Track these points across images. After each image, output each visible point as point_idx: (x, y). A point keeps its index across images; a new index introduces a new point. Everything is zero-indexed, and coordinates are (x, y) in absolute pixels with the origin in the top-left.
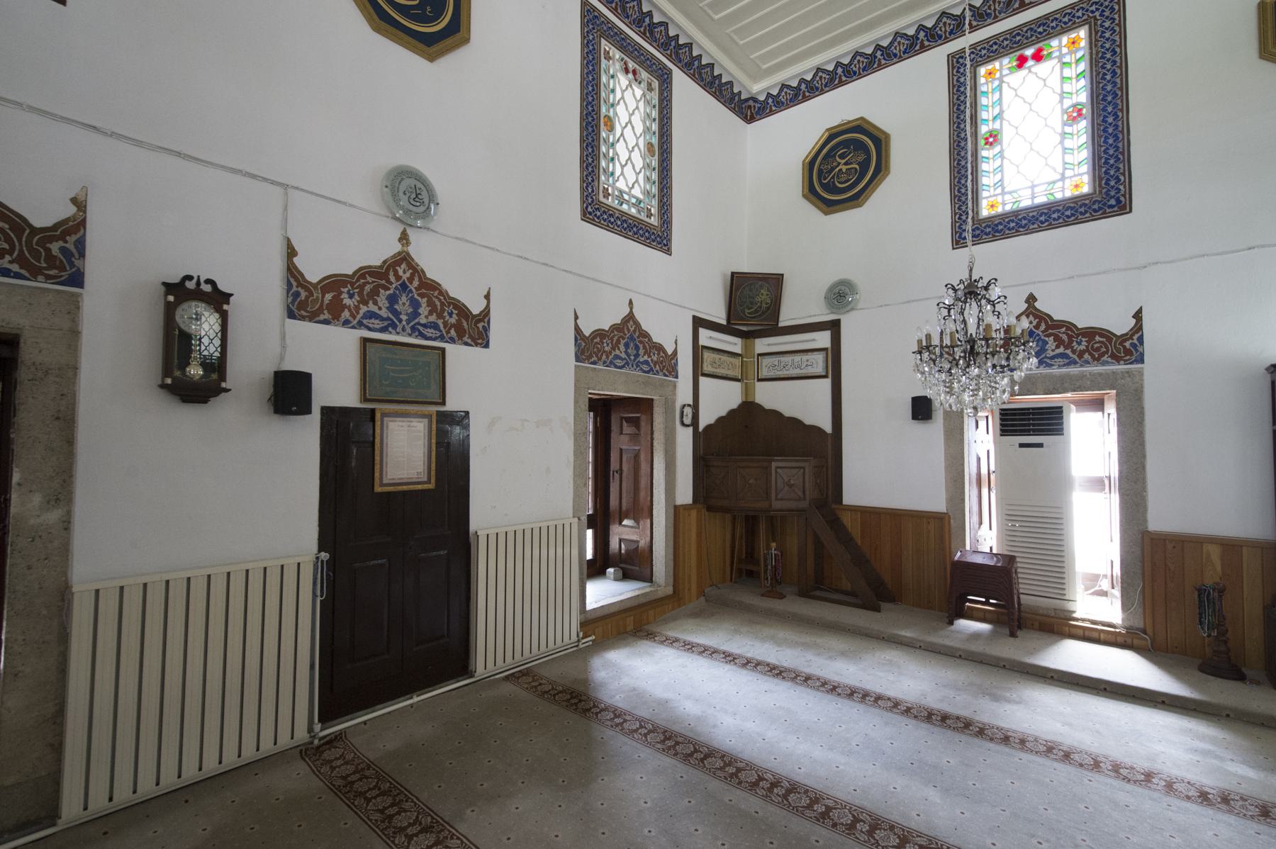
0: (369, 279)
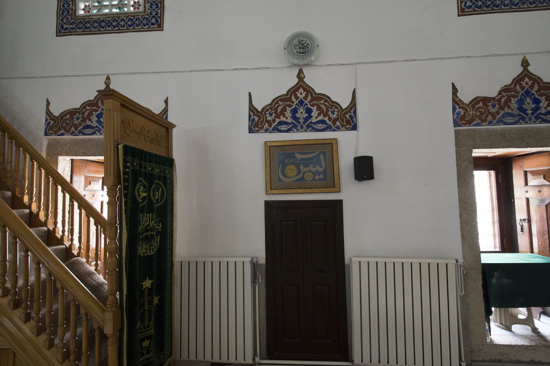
0: (280, 103)
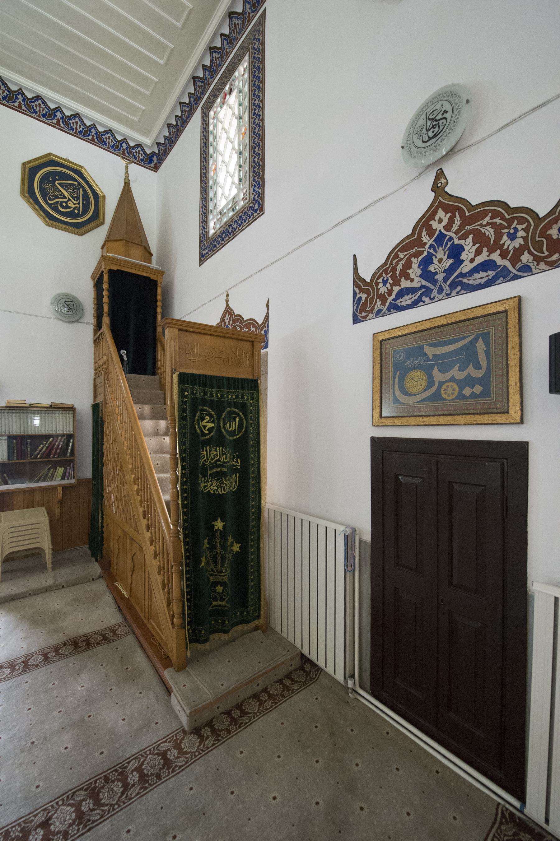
0: (401, 255)
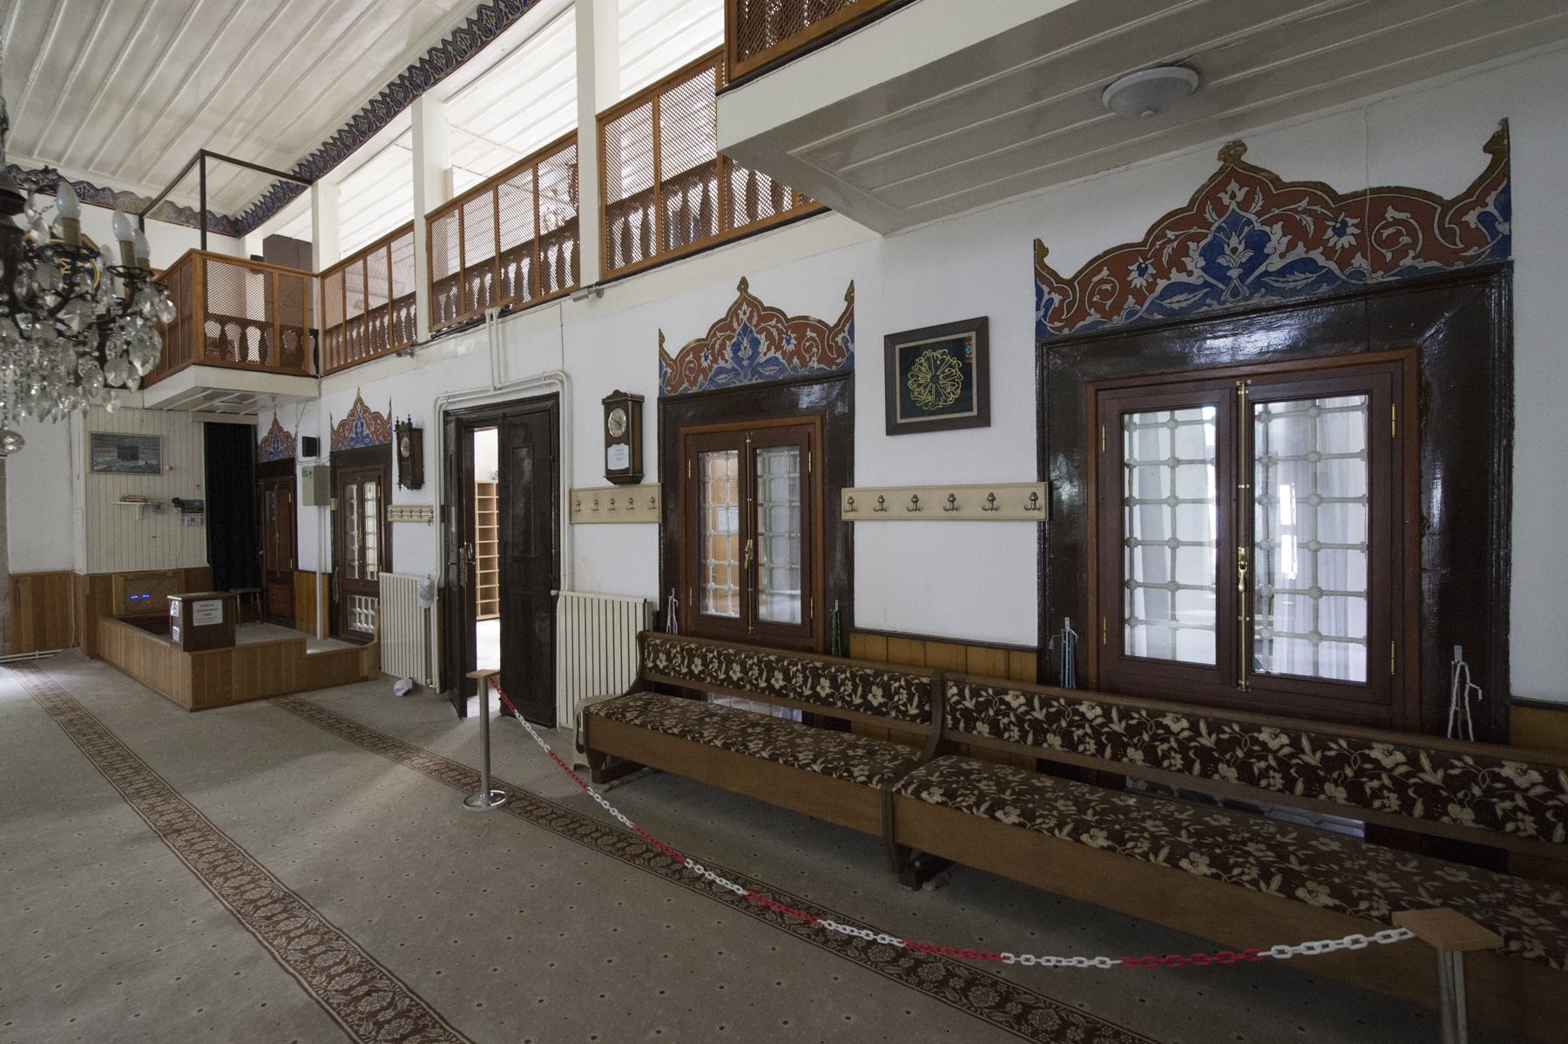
0: (1170, 234)
